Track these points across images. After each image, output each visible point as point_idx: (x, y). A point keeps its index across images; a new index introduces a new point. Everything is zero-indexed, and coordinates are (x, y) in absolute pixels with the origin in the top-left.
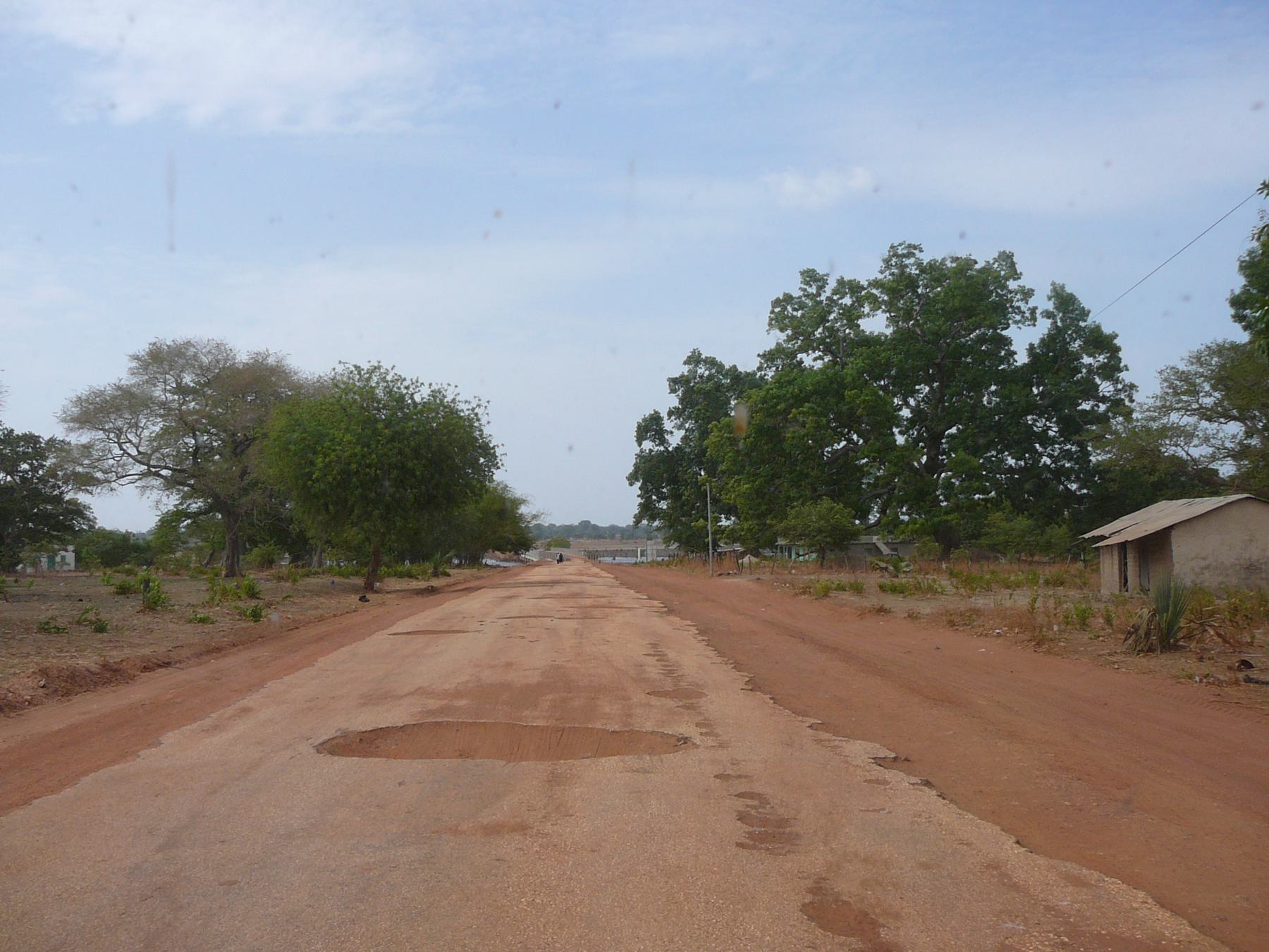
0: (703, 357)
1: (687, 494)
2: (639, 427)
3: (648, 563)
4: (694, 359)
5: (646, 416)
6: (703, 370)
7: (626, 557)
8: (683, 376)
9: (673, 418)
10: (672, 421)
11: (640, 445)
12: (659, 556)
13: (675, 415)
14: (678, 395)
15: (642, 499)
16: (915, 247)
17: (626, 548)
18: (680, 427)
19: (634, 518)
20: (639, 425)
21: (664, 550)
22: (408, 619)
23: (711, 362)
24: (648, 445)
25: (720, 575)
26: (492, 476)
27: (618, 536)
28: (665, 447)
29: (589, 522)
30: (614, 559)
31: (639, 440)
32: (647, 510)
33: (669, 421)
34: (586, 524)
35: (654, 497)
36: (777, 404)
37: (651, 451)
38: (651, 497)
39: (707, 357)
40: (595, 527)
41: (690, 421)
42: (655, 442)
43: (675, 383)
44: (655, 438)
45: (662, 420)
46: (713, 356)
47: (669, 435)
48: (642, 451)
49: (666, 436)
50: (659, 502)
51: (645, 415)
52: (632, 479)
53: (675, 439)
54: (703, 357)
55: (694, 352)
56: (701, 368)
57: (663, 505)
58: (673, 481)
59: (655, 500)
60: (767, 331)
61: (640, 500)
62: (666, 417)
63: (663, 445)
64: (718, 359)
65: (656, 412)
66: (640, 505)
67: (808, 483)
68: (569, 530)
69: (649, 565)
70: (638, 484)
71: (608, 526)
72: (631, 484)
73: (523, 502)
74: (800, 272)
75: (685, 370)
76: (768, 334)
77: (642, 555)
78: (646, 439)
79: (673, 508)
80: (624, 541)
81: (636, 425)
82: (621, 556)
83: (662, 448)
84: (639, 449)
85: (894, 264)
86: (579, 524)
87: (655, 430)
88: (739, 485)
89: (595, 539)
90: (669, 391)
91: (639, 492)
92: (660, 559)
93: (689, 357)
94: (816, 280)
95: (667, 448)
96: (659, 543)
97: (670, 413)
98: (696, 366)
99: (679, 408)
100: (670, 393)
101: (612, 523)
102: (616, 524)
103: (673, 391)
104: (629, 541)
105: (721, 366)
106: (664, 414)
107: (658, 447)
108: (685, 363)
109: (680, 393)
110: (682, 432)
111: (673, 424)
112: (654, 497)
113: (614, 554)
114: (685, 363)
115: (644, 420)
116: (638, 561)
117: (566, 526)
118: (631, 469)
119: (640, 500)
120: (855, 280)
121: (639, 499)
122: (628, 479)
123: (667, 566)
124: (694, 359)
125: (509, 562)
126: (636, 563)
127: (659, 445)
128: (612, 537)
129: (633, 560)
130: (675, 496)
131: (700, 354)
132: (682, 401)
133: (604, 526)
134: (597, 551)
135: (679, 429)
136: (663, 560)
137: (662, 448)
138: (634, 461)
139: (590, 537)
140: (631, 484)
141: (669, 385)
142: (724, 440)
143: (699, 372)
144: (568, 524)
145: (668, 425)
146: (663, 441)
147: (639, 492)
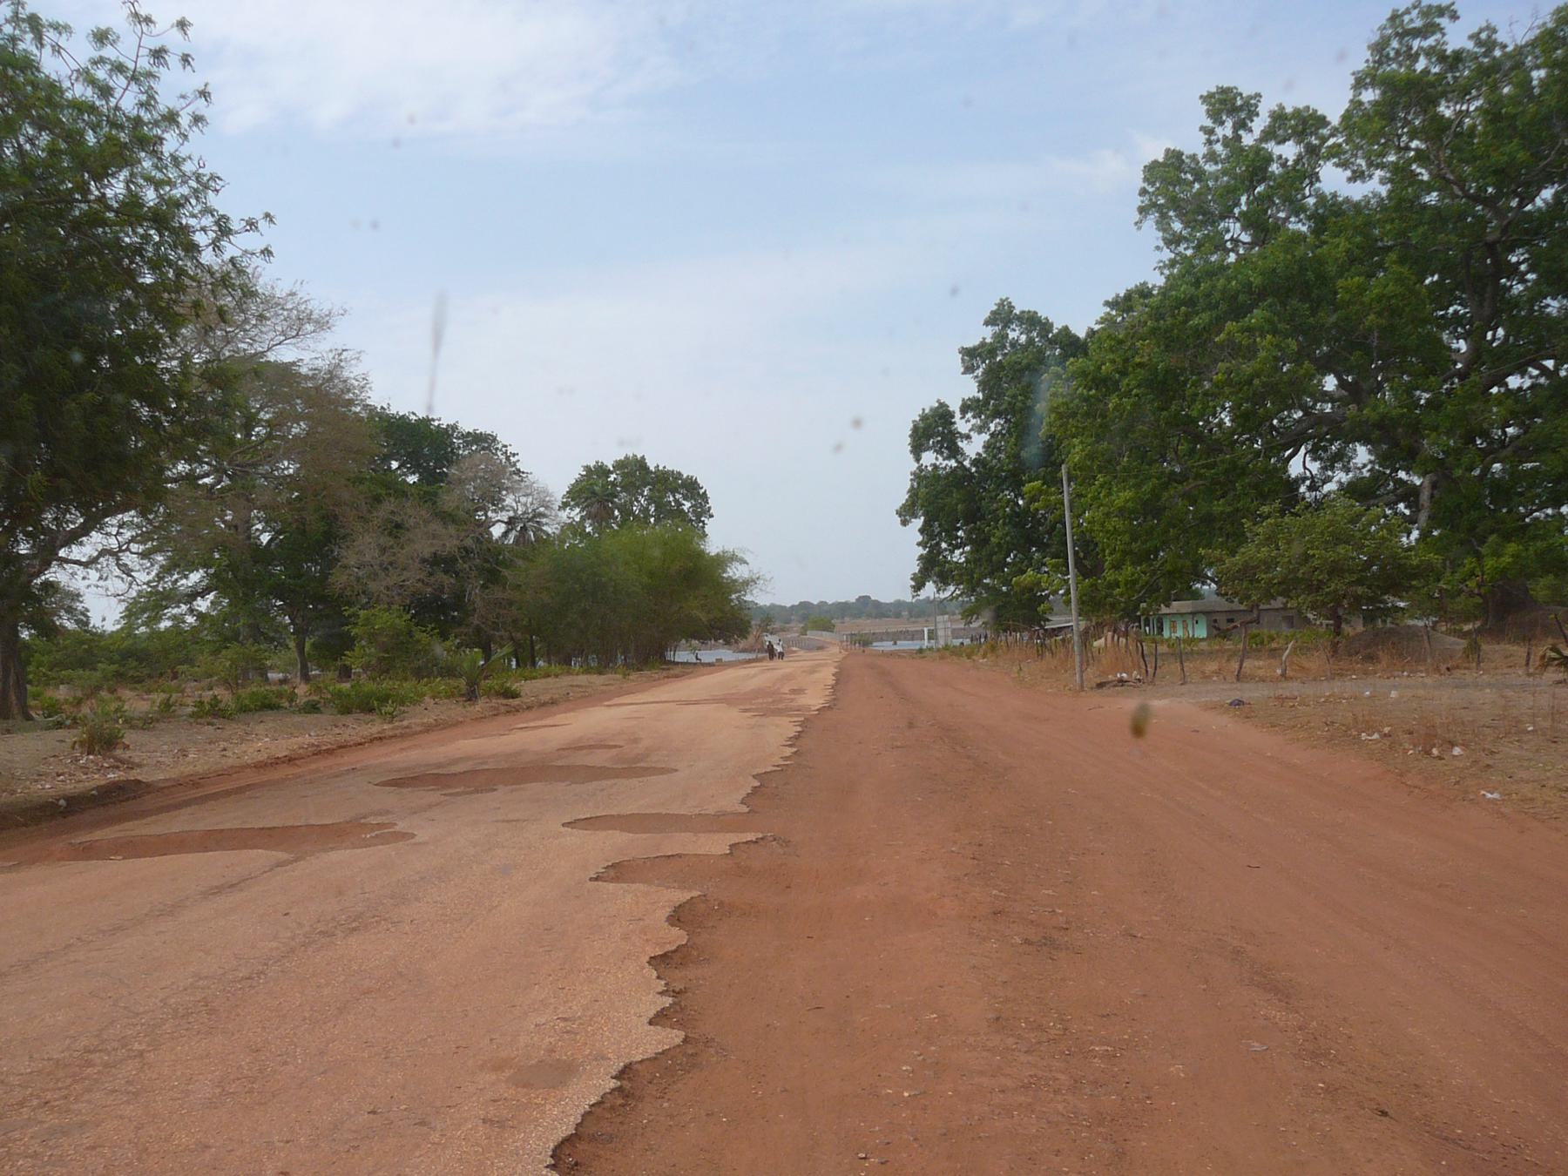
0: (1017, 311)
1: (998, 534)
2: (915, 429)
3: (938, 650)
4: (1003, 316)
5: (927, 411)
6: (1017, 333)
7: (913, 640)
8: (983, 344)
9: (969, 415)
10: (968, 421)
11: (918, 459)
12: (957, 638)
13: (972, 410)
14: (977, 377)
15: (925, 547)
16: (1441, 11)
17: (912, 628)
18: (980, 429)
19: (912, 579)
20: (915, 426)
21: (964, 629)
22: (404, 790)
23: (1031, 321)
24: (929, 458)
25: (1100, 685)
26: (703, 527)
27: (905, 613)
28: (957, 461)
29: (869, 597)
30: (895, 643)
31: (917, 449)
32: (932, 567)
33: (963, 421)
34: (864, 600)
35: (944, 545)
36: (1188, 317)
37: (935, 467)
38: (938, 544)
39: (1023, 312)
40: (877, 604)
41: (998, 420)
42: (942, 453)
43: (971, 356)
44: (941, 448)
45: (953, 417)
46: (1032, 309)
47: (965, 442)
48: (920, 468)
49: (960, 444)
50: (952, 552)
51: (924, 410)
52: (906, 513)
53: (974, 447)
54: (1017, 311)
55: (1001, 304)
56: (1014, 330)
57: (958, 556)
58: (973, 516)
59: (946, 550)
60: (1136, 223)
61: (921, 551)
62: (958, 415)
63: (955, 457)
64: (1042, 314)
65: (942, 405)
66: (921, 558)
67: (1249, 485)
68: (843, 609)
69: (936, 655)
70: (918, 522)
71: (892, 601)
72: (904, 523)
73: (733, 558)
74: (1201, 97)
75: (988, 334)
76: (1139, 228)
77: (930, 638)
78: (928, 449)
79: (976, 561)
80: (913, 619)
81: (911, 425)
82: (905, 639)
83: (953, 463)
84: (917, 465)
85: (1392, 54)
86: (857, 600)
87: (942, 434)
88: (1109, 494)
89: (876, 618)
90: (962, 370)
91: (920, 538)
92: (957, 642)
93: (993, 313)
94: (1233, 110)
95: (961, 463)
96: (957, 620)
97: (965, 409)
98: (1006, 326)
99: (978, 400)
100: (963, 373)
101: (898, 598)
102: (902, 599)
103: (969, 369)
104: (920, 619)
105: (1045, 326)
106: (955, 406)
107: (946, 462)
108: (987, 323)
109: (979, 372)
110: (986, 437)
111: (969, 425)
112: (944, 545)
113: (895, 637)
114: (987, 323)
115: (924, 418)
116: (924, 647)
117: (840, 603)
118: (902, 497)
119: (921, 551)
120: (1308, 107)
121: (921, 548)
122: (899, 513)
123: (969, 657)
124: (1003, 316)
125: (750, 652)
126: (921, 651)
127: (948, 458)
128: (898, 615)
129: (914, 645)
130: (979, 542)
131: (1011, 307)
132: (983, 385)
133: (888, 602)
134: (874, 634)
135: (980, 433)
136: (962, 644)
137: (953, 463)
138: (908, 486)
139: (869, 616)
140: (904, 523)
141: (963, 359)
142: (1076, 401)
143: (1010, 337)
144: (843, 601)
145: (962, 426)
146: (954, 452)
147: (920, 538)
